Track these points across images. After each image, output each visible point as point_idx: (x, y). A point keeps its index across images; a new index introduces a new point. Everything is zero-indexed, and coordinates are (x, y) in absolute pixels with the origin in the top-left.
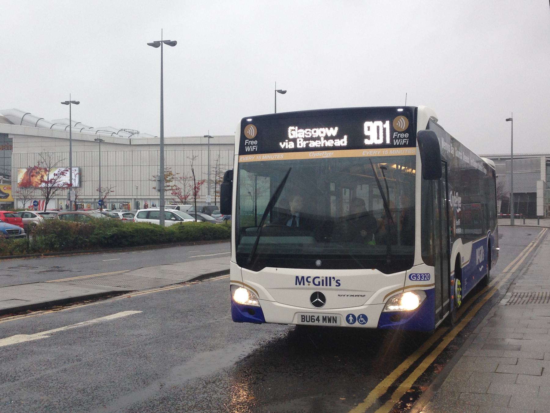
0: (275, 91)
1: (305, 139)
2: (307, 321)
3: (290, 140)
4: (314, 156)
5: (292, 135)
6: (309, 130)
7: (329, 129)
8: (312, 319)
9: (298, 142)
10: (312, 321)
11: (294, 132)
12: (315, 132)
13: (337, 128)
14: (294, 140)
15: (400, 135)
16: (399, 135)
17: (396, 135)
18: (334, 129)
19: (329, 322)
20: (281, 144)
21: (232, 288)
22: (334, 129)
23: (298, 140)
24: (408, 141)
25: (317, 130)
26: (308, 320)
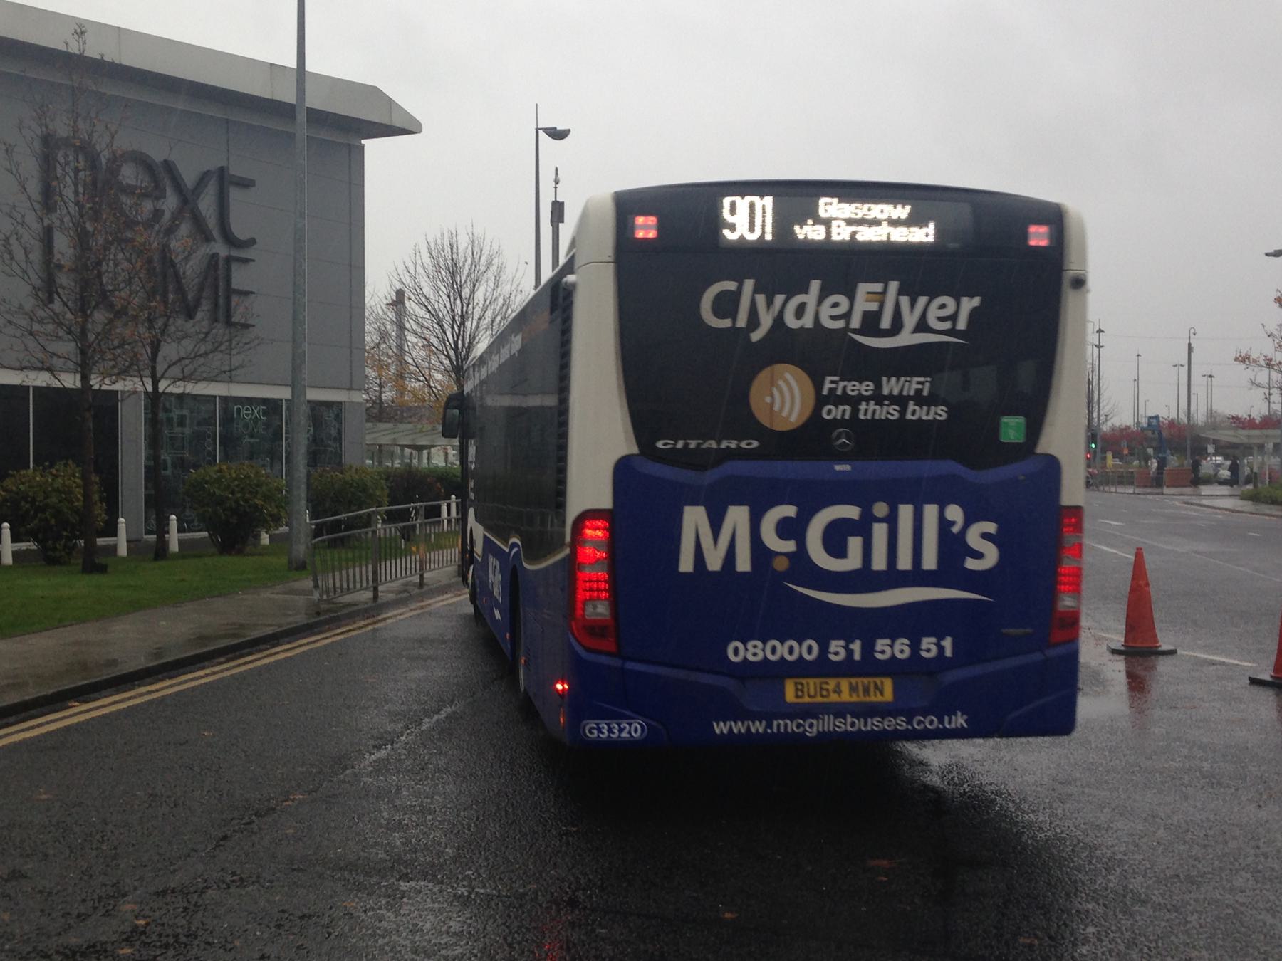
0: (537, 130)
1: (850, 222)
2: (810, 696)
3: (818, 221)
4: (754, 321)
5: (826, 211)
6: (858, 205)
7: (895, 207)
8: (822, 689)
9: (834, 230)
10: (822, 696)
11: (829, 207)
12: (869, 210)
13: (908, 207)
14: (827, 223)
15: (845, 387)
16: (842, 384)
17: (833, 386)
18: (903, 208)
19: (864, 696)
20: (797, 228)
21: (595, 629)
22: (903, 208)
23: (834, 223)
24: (927, 385)
25: (873, 206)
26: (812, 693)
